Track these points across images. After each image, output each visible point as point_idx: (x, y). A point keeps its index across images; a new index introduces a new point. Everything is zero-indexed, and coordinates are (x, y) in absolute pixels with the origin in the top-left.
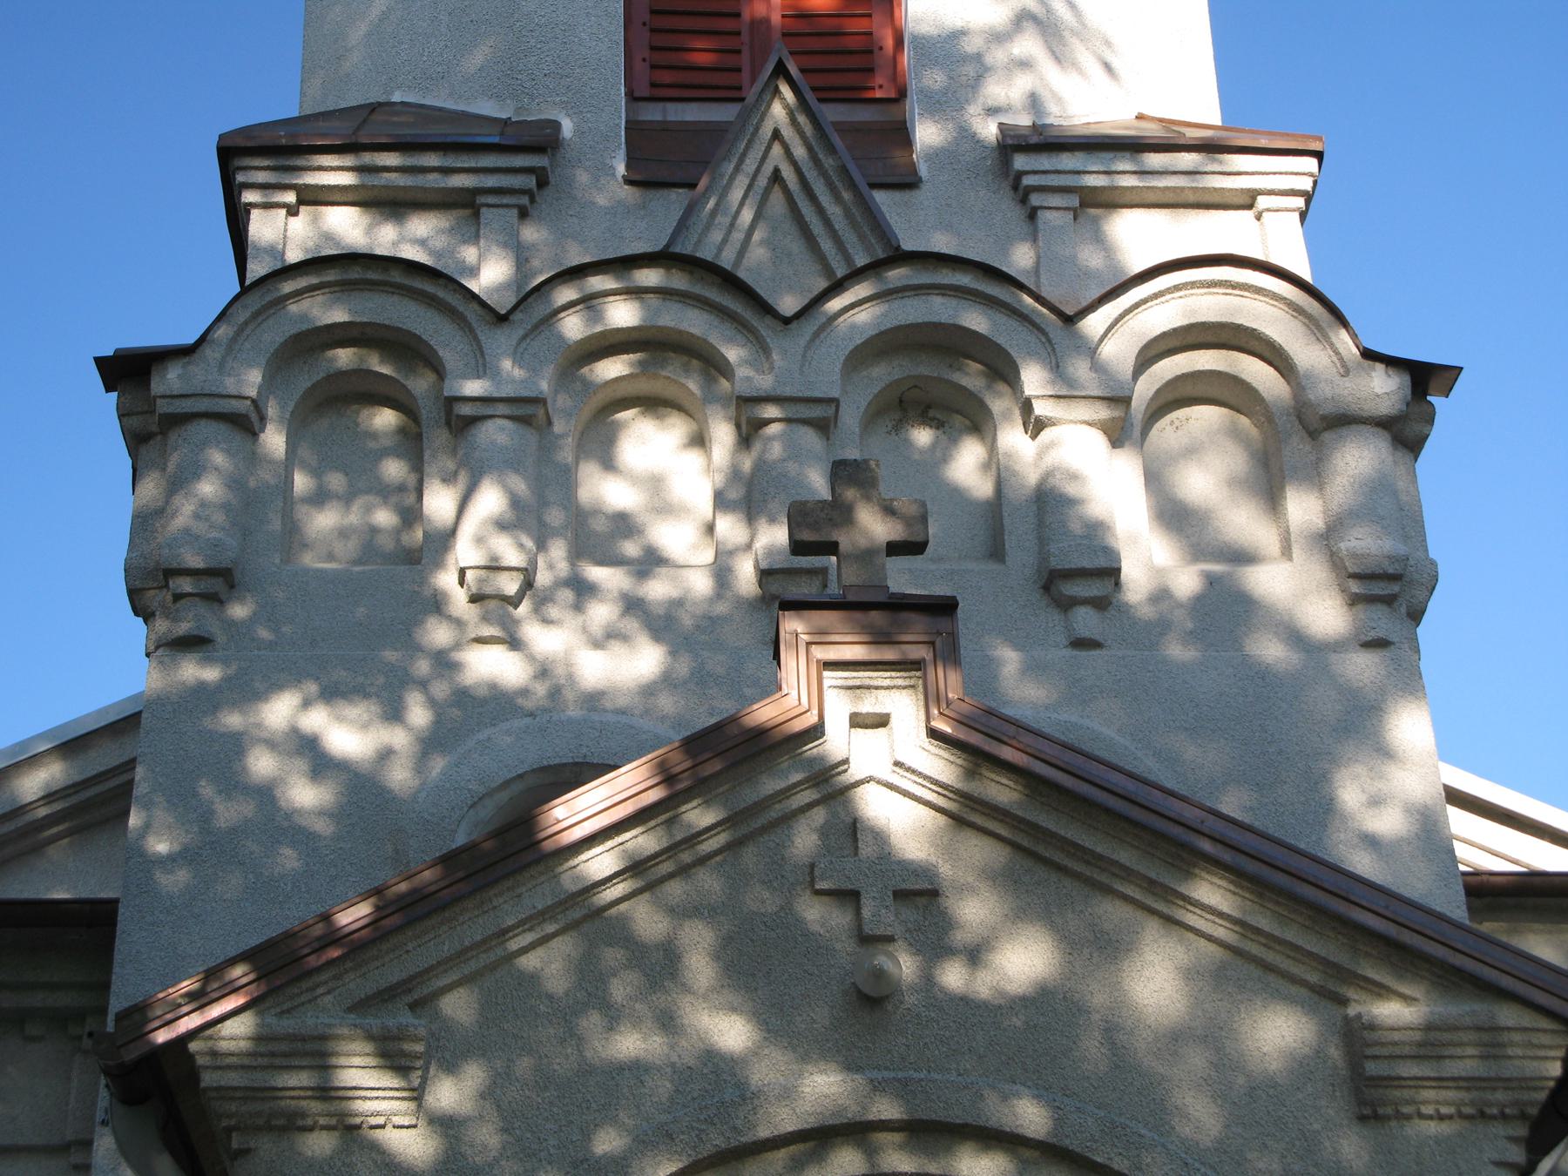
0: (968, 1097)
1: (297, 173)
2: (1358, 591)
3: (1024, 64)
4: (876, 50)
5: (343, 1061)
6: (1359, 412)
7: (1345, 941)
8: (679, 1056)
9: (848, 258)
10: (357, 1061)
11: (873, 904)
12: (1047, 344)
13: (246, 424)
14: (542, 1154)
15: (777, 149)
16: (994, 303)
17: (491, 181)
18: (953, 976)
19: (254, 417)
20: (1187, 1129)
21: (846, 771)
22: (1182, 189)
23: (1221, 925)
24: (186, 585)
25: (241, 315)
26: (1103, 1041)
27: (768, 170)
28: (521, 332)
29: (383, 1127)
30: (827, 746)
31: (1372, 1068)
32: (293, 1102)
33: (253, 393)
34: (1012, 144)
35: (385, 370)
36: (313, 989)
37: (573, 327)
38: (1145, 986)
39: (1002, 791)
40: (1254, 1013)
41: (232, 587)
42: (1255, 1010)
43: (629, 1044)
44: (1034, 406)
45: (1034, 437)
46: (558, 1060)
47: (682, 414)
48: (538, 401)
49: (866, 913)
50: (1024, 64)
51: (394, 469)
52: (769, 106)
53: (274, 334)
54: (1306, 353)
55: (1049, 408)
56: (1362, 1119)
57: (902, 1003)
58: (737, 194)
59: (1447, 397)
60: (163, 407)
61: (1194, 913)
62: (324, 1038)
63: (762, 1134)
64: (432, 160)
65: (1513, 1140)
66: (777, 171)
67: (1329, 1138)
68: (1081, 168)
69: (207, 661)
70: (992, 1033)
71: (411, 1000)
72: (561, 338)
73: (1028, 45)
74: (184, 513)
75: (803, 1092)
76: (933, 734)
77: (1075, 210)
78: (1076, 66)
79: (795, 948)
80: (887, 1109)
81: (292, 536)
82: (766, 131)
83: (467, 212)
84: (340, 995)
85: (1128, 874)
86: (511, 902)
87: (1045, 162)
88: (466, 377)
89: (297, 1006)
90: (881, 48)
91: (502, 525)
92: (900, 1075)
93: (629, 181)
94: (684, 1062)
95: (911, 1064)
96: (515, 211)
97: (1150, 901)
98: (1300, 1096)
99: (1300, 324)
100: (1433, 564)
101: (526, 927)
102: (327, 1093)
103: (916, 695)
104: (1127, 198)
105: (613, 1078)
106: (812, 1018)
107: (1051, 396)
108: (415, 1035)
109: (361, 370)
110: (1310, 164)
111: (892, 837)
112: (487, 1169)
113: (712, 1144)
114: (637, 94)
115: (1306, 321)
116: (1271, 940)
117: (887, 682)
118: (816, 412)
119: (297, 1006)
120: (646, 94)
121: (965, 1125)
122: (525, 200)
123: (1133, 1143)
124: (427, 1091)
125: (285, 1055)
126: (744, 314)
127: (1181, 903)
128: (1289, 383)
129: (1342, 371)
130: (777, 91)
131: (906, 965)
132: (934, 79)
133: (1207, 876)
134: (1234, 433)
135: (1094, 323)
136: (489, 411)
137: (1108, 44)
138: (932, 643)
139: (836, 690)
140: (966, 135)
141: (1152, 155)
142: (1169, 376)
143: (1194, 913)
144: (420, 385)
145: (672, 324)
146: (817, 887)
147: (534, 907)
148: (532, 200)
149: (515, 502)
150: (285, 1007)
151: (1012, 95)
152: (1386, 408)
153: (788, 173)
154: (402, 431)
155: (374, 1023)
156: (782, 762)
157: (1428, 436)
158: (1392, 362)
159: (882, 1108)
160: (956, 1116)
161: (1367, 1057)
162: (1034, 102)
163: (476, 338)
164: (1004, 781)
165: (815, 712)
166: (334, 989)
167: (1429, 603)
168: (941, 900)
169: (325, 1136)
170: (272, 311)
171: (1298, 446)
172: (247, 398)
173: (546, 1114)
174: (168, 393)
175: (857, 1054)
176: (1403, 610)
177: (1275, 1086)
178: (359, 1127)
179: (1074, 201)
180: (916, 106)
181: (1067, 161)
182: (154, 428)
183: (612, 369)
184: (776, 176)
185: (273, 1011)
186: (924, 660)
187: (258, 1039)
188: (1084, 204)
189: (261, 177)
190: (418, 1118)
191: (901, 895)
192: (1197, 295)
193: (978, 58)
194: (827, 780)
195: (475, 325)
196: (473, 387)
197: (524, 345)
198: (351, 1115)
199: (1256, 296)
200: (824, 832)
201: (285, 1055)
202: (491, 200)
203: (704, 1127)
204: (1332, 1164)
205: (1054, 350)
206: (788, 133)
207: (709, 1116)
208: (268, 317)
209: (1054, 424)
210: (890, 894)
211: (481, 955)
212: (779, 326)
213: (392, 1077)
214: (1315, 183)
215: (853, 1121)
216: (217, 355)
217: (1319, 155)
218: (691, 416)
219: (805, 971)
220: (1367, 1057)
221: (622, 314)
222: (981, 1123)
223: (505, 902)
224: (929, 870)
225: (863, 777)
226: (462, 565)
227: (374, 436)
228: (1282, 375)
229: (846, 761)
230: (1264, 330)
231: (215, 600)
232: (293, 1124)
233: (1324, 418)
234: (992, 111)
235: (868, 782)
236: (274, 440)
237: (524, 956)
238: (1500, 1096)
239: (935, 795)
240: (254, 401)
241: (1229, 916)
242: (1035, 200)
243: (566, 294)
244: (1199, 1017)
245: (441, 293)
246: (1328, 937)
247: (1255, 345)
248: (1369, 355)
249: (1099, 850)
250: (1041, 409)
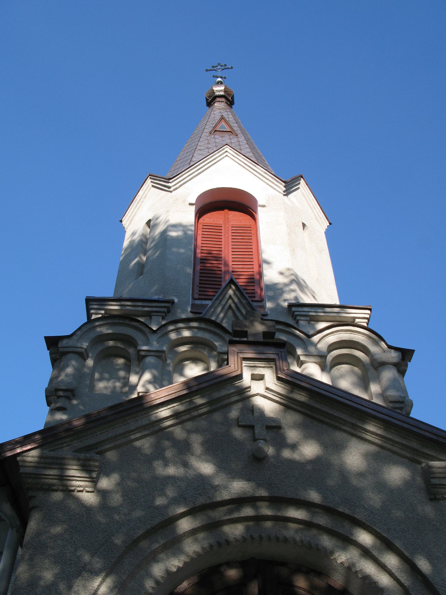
0: (293, 489)
1: (105, 306)
2: (392, 406)
3: (293, 291)
4: (256, 293)
5: (70, 467)
6: (389, 361)
7: (419, 443)
8: (190, 474)
10: (75, 467)
11: (259, 429)
12: (303, 343)
13: (83, 356)
14: (139, 504)
15: (230, 301)
16: (288, 333)
17: (155, 309)
18: (287, 454)
20: (371, 503)
21: (249, 391)
22: (336, 316)
23: (377, 439)
24: (61, 393)
25: (85, 329)
26: (339, 474)
27: (228, 305)
28: (160, 336)
29: (82, 491)
30: (244, 382)
31: (433, 481)
32: (51, 480)
33: (85, 347)
34: (291, 306)
35: (122, 347)
36: (63, 444)
37: (173, 336)
38: (353, 458)
39: (301, 397)
40: (390, 466)
41: (74, 396)
42: (391, 466)
43: (171, 471)
44: (300, 357)
45: (300, 368)
46: (146, 474)
47: (203, 362)
48: (163, 352)
49: (256, 431)
50: (293, 291)
51: (122, 373)
52: (228, 290)
53: (92, 335)
54: (373, 349)
55: (304, 358)
56: (431, 500)
57: (269, 461)
58: (219, 309)
59: (410, 362)
60: (61, 350)
61: (368, 435)
62: (64, 459)
63: (218, 499)
64: (140, 304)
66: (230, 306)
67: (420, 506)
68: (310, 311)
69: (65, 413)
70: (301, 471)
71: (97, 451)
72: (170, 339)
73: (294, 286)
74: (62, 377)
75: (234, 486)
76: (279, 379)
78: (306, 294)
79: (232, 443)
80: (263, 493)
81: (92, 387)
82: (227, 296)
83: (148, 318)
84: (72, 447)
85: (345, 422)
86: (134, 422)
87: (300, 309)
88: (144, 345)
89: (56, 449)
90: (257, 293)
91: (150, 382)
93: (191, 312)
94: (192, 476)
95: (272, 480)
96: (161, 317)
97: (353, 431)
98: (409, 493)
99: (371, 341)
100: (411, 401)
101: (139, 431)
102: (63, 478)
103: (273, 369)
104: (322, 319)
105: (166, 480)
106: (237, 464)
107: (305, 355)
108: (96, 459)
109: (116, 346)
110: (369, 312)
111: (265, 411)
112: (118, 508)
113: (200, 502)
114: (195, 298)
115: (372, 340)
116: (394, 442)
117: (263, 365)
119: (56, 449)
120: (197, 298)
121: (292, 499)
122: (164, 314)
123: (352, 505)
124: (99, 481)
125: (50, 464)
126: (221, 333)
127: (363, 432)
128: (368, 357)
129: (383, 352)
130: (231, 287)
131: (270, 451)
132: (270, 293)
133: (371, 423)
134: (353, 372)
135: (315, 339)
136: (149, 354)
137: (314, 292)
138: (278, 354)
139: (247, 367)
140: (278, 305)
141: (328, 308)
142: (336, 355)
143: (368, 435)
144: (131, 351)
145: (201, 336)
146: (240, 424)
147: (142, 424)
148: (166, 315)
149: (154, 377)
150: (52, 449)
151: (291, 297)
152: (395, 360)
153: (233, 306)
154: (125, 364)
155: (82, 456)
156: (228, 386)
157: (406, 370)
158: (396, 349)
159: (262, 492)
160: (289, 495)
161: (431, 478)
162: (296, 298)
163: (147, 337)
164: (303, 394)
165: (240, 371)
166: (70, 445)
167: (411, 411)
168: (282, 431)
169: (61, 494)
170: (93, 329)
171: (372, 371)
172: (83, 348)
173: (141, 491)
174: (63, 346)
175: (253, 476)
177: (400, 489)
178: (73, 491)
179: (308, 319)
180: (266, 298)
181: (306, 309)
182: (58, 357)
183: (183, 349)
184: (230, 307)
185: (48, 450)
186: (275, 359)
187: (40, 457)
188: (311, 320)
189: (96, 307)
190: (95, 489)
191: (269, 428)
192: (343, 333)
193: (281, 289)
194: (243, 393)
195: (147, 333)
196: (145, 348)
197: (160, 339)
198: (71, 486)
199: (358, 334)
200: (242, 410)
201: (50, 464)
202: (155, 314)
203: (197, 496)
204: (422, 514)
205: (305, 344)
206: (233, 297)
207: (199, 493)
208: (92, 331)
209: (306, 363)
210: (265, 426)
211: (122, 439)
213: (87, 473)
214: (370, 316)
215: (251, 496)
216: (77, 338)
217: (370, 310)
218: (205, 363)
219: (235, 450)
220: (431, 478)
221: (186, 334)
222: (298, 498)
223: (132, 422)
224: (278, 420)
225: (256, 393)
226: (139, 391)
227: (118, 365)
228: (366, 354)
229: (249, 387)
230: (361, 342)
231: (69, 398)
232: (50, 489)
234: (285, 300)
235: (257, 395)
236: (90, 362)
237: (138, 441)
239: (280, 399)
240: (85, 349)
241: (380, 435)
242: (298, 318)
243: (171, 328)
244: (372, 467)
246: (413, 441)
247: (359, 347)
248: (390, 347)
249: (335, 414)
250: (302, 358)
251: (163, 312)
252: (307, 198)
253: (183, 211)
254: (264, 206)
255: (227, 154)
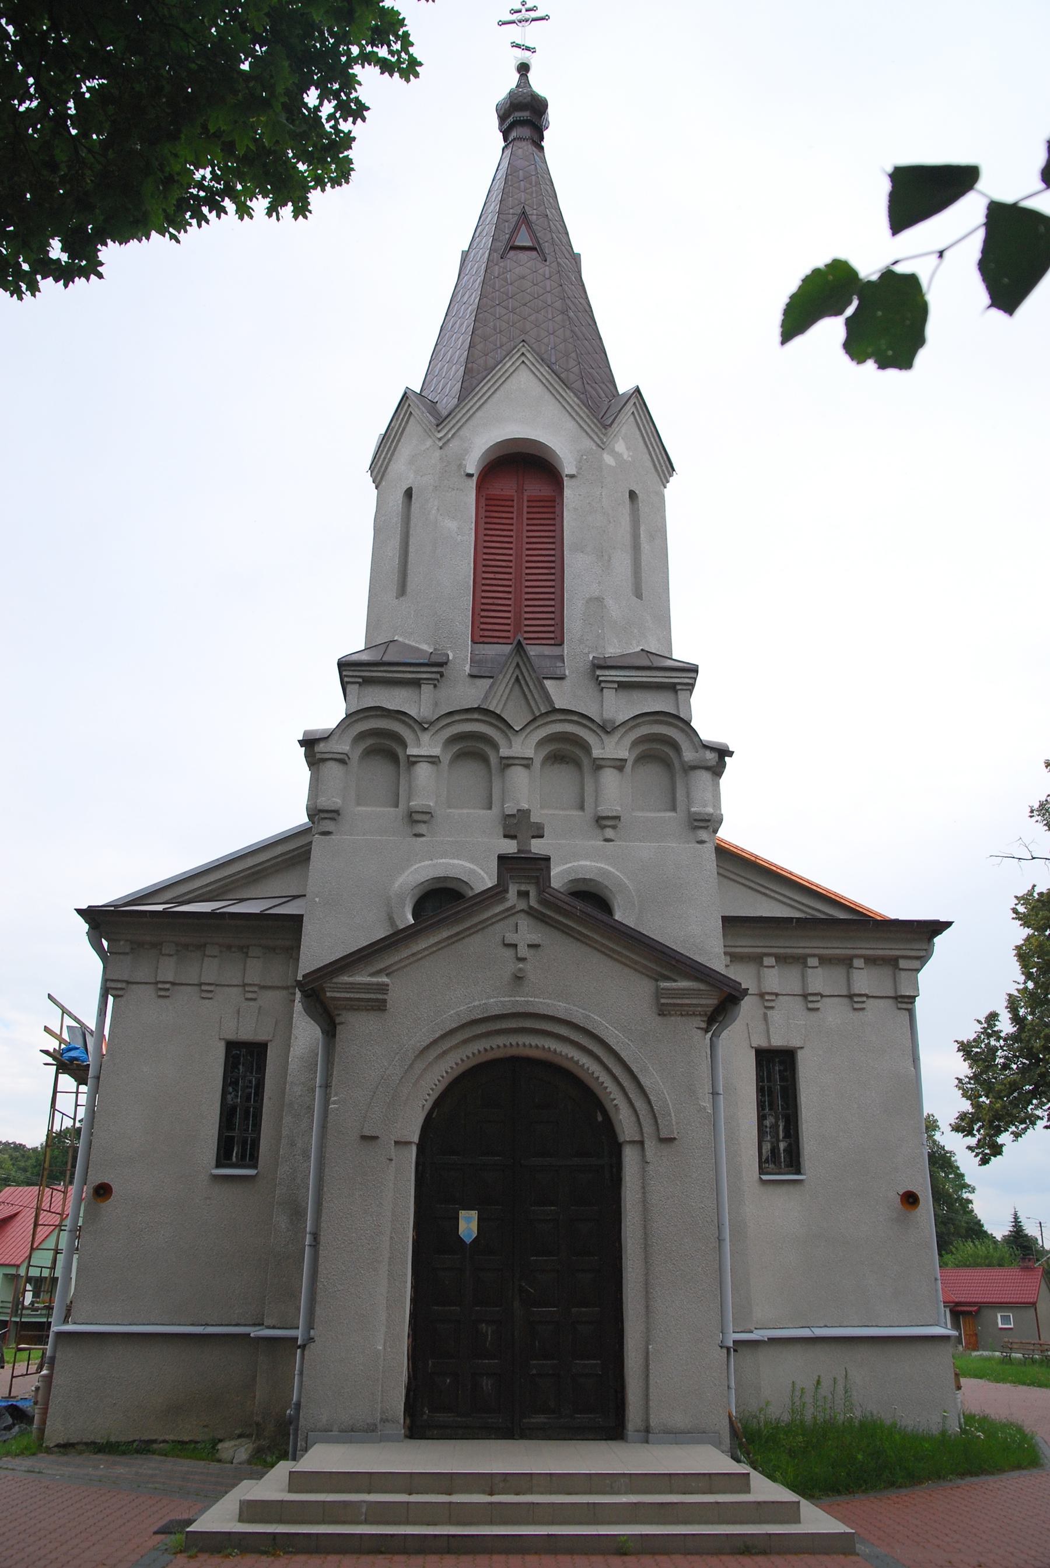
9: (539, 709)
19: (346, 758)
56: (659, 1015)
60: (318, 756)
65: (703, 1021)
77: (616, 688)
92: (526, 999)
96: (432, 686)
118: (525, 762)
122: (436, 682)
176: (711, 830)
197: (420, 1066)
202: (425, 682)
210: (393, 1143)
212: (515, 732)
233: (690, 766)
238: (699, 1009)
245: (407, 720)
251: (435, 679)
252: (644, 432)
253: (457, 489)
254: (572, 476)
255: (523, 358)
